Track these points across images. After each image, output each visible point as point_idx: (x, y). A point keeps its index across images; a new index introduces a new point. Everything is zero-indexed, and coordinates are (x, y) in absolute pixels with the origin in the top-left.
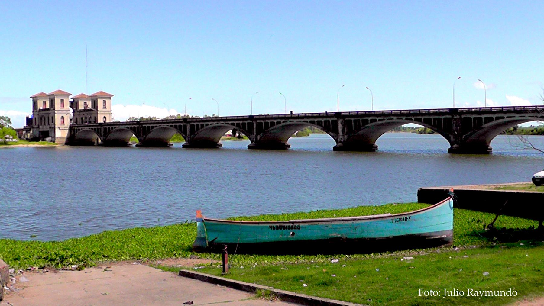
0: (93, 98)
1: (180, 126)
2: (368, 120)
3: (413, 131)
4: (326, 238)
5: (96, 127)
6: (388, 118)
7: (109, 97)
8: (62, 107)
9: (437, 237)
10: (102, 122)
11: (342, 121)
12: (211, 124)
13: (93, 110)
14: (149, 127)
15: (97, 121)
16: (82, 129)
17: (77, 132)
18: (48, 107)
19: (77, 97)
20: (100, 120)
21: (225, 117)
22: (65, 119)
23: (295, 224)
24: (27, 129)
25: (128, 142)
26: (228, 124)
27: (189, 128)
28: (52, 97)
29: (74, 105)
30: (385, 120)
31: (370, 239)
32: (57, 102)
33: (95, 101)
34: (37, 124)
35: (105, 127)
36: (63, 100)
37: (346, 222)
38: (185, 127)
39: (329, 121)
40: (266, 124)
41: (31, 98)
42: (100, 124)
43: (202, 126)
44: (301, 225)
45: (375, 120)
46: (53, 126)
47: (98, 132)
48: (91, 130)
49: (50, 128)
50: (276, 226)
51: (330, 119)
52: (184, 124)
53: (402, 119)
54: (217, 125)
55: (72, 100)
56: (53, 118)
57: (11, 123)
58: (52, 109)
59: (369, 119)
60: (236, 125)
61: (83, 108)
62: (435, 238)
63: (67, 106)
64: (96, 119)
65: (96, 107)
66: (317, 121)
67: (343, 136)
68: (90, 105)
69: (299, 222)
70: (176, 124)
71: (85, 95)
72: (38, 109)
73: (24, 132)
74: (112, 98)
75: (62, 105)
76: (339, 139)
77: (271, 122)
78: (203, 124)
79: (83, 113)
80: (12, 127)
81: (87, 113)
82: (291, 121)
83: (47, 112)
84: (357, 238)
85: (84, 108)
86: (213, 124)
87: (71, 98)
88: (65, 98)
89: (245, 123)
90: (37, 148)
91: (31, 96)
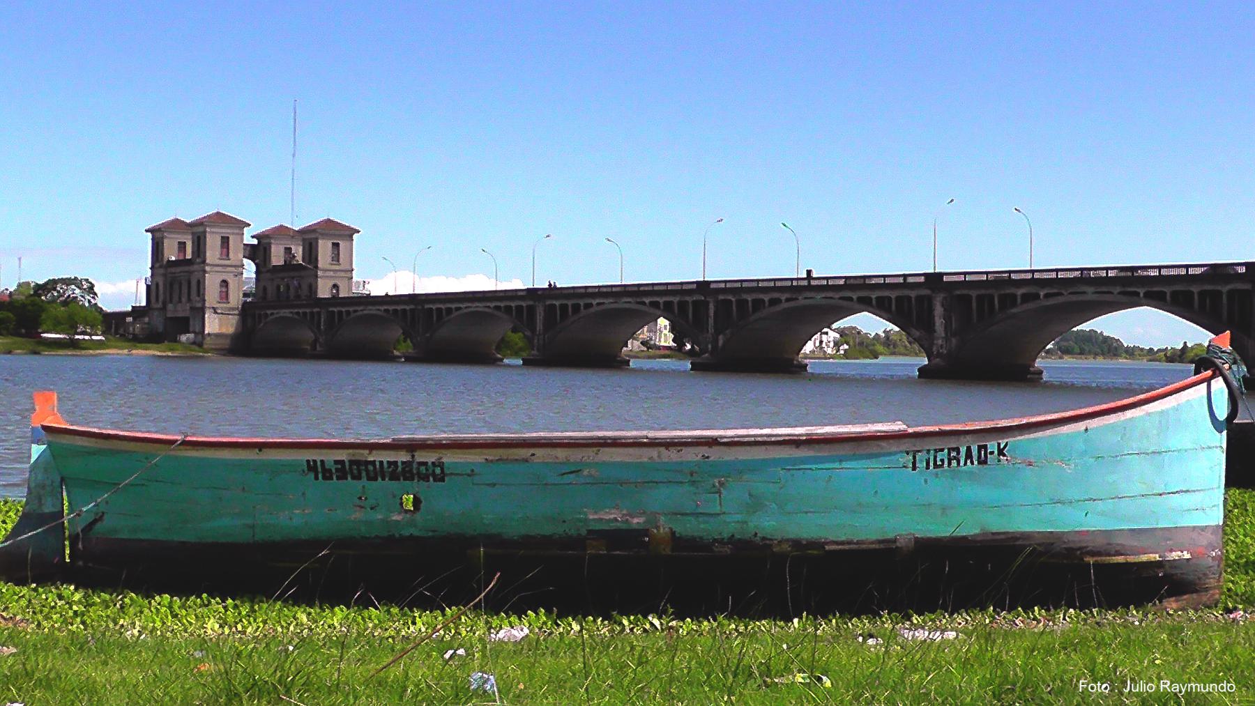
0: (307, 236)
1: (519, 308)
2: (1014, 296)
3: (1149, 357)
4: (573, 532)
7: (349, 233)
8: (224, 257)
9: (1144, 558)
11: (945, 298)
12: (598, 304)
14: (439, 310)
16: (272, 314)
17: (260, 322)
18: (189, 256)
19: (267, 233)
20: (324, 292)
22: (231, 286)
23: (421, 457)
26: (644, 303)
27: (542, 314)
28: (200, 229)
29: (261, 253)
30: (1061, 294)
31: (797, 543)
33: (311, 244)
34: (161, 298)
36: (228, 238)
37: (672, 455)
38: (531, 310)
39: (909, 298)
40: (742, 304)
41: (147, 231)
43: (576, 308)
44: (449, 458)
46: (199, 305)
48: (296, 317)
49: (192, 309)
50: (336, 462)
51: (913, 294)
52: (531, 303)
53: (1112, 293)
56: (200, 284)
57: (96, 294)
59: (1020, 292)
60: (662, 307)
61: (282, 263)
62: (1131, 559)
64: (313, 289)
65: (313, 260)
66: (877, 298)
67: (947, 339)
68: (298, 251)
69: (438, 446)
70: (508, 303)
72: (165, 260)
73: (130, 319)
74: (355, 236)
75: (225, 250)
76: (934, 349)
78: (579, 305)
79: (282, 275)
80: (100, 305)
81: (292, 274)
82: (806, 298)
83: (186, 268)
84: (726, 535)
85: (285, 261)
86: (603, 303)
87: (253, 237)
88: (233, 234)
89: (687, 302)
90: (154, 356)
91: (147, 228)
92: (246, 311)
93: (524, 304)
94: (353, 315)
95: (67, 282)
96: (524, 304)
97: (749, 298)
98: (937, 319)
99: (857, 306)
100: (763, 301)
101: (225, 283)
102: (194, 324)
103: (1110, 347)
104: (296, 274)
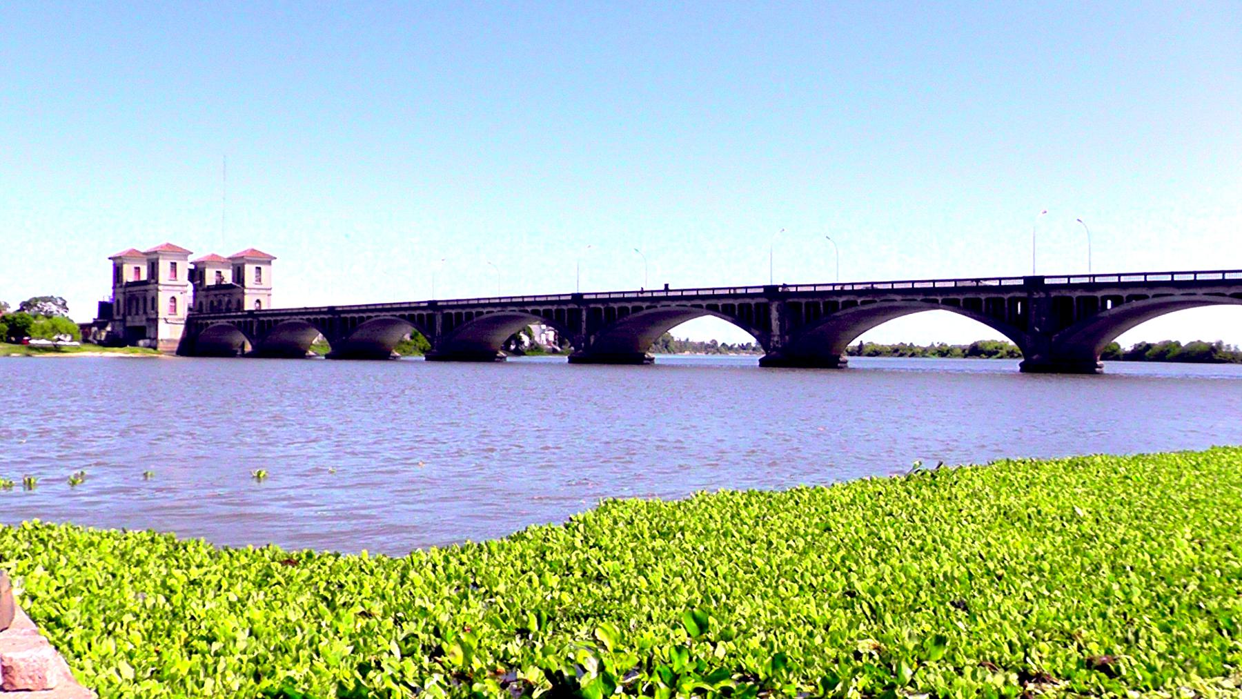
0: (236, 262)
1: (421, 316)
2: (837, 303)
5: (241, 320)
6: (882, 298)
7: (268, 260)
10: (253, 308)
12: (488, 313)
13: (235, 287)
15: (243, 307)
17: (202, 329)
18: (144, 276)
20: (249, 305)
21: (972, 280)
24: (99, 324)
25: (306, 352)
26: (527, 311)
28: (155, 256)
30: (875, 302)
32: (164, 267)
33: (239, 268)
34: (122, 311)
35: (261, 319)
40: (610, 311)
42: (250, 312)
45: (854, 303)
46: (154, 316)
47: (246, 329)
49: (148, 320)
51: (753, 302)
54: (500, 314)
55: (192, 267)
56: (154, 301)
58: (153, 281)
59: (841, 300)
61: (214, 283)
63: (183, 276)
64: (240, 304)
67: (781, 336)
68: (228, 277)
71: (217, 256)
72: (125, 281)
74: (273, 262)
77: (620, 308)
79: (213, 292)
81: (223, 292)
83: (143, 288)
92: (191, 323)
93: (424, 313)
94: (211, 326)
95: (46, 300)
96: (424, 313)
97: (616, 306)
98: (773, 322)
99: (705, 311)
100: (627, 308)
101: (174, 299)
102: (150, 333)
103: (684, 346)
104: (227, 291)
